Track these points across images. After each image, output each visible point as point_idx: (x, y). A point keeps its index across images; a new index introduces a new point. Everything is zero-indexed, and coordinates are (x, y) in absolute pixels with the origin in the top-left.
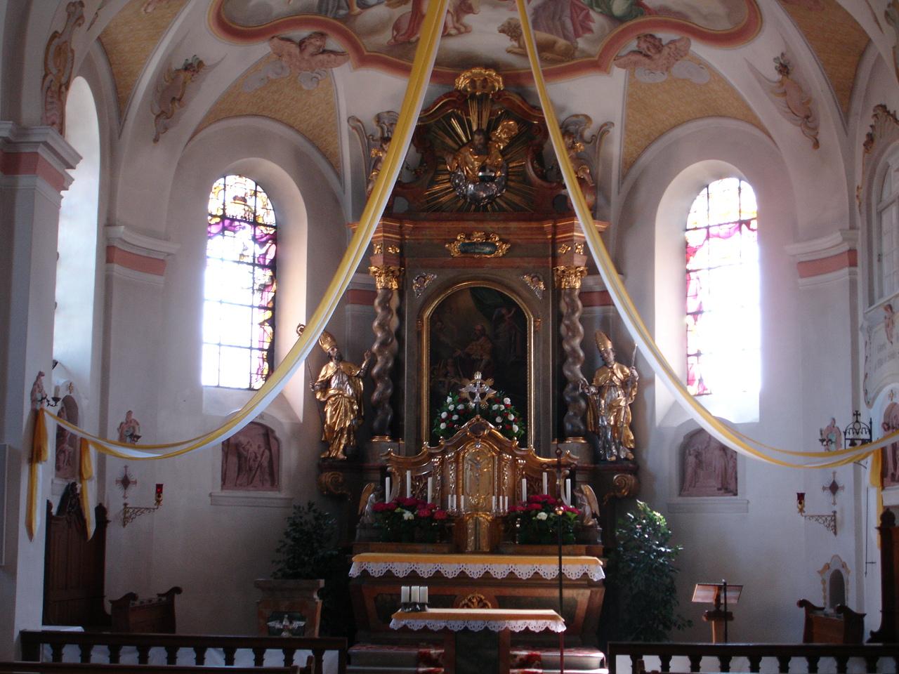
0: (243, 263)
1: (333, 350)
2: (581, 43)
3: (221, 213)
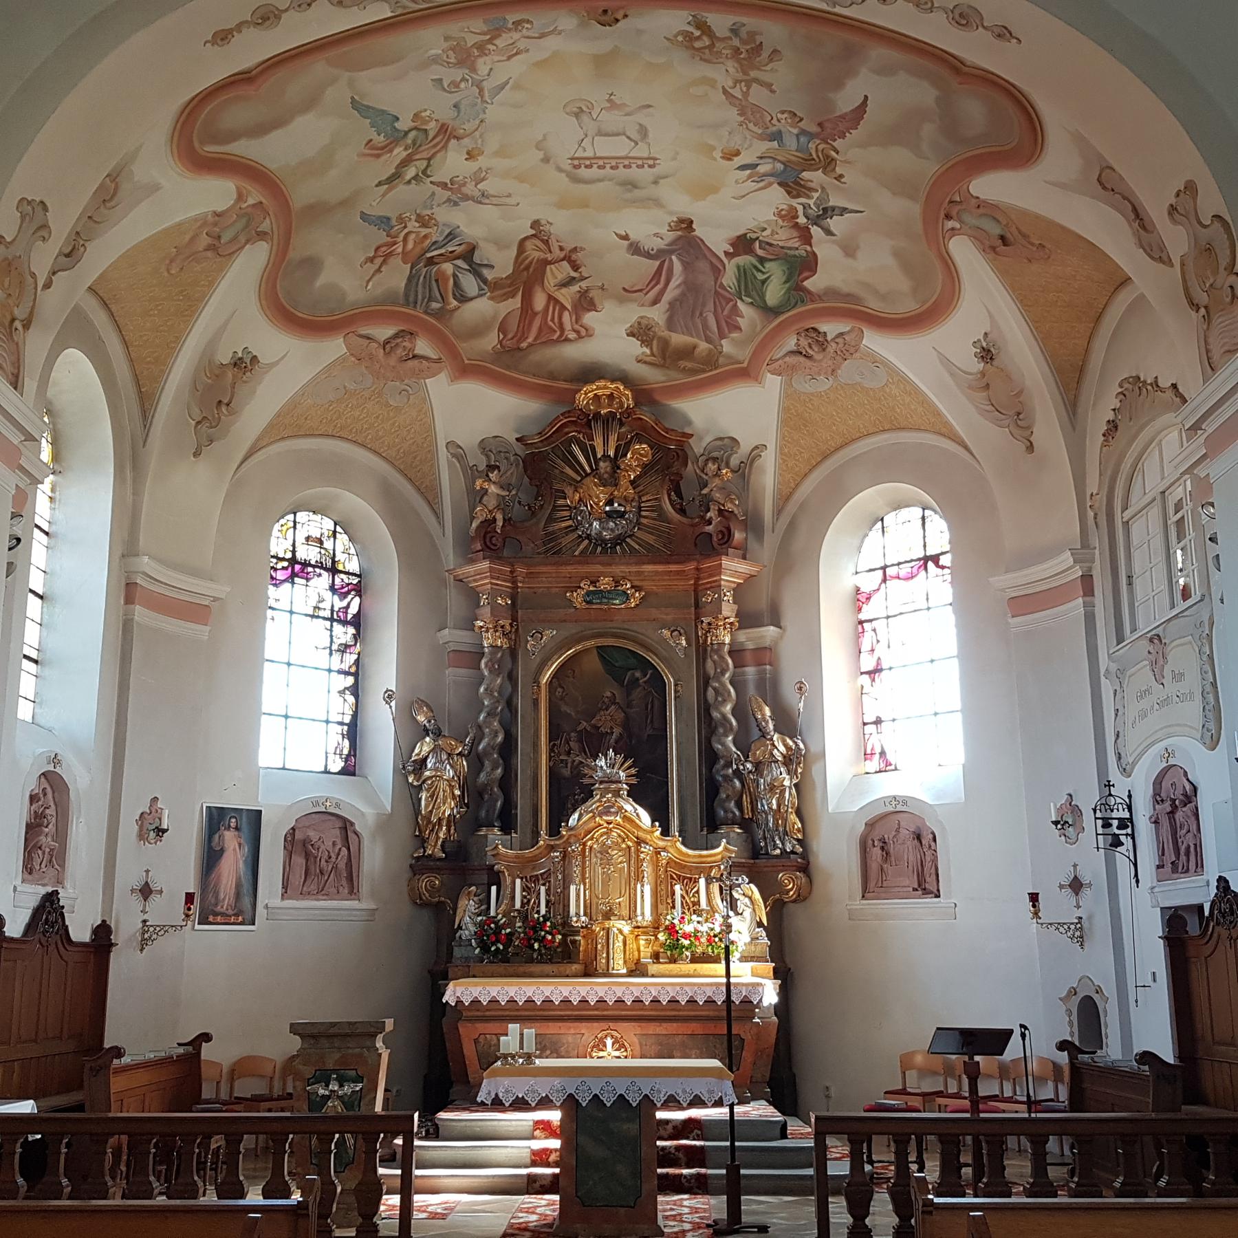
0: (318, 617)
2: (727, 346)
3: (289, 555)
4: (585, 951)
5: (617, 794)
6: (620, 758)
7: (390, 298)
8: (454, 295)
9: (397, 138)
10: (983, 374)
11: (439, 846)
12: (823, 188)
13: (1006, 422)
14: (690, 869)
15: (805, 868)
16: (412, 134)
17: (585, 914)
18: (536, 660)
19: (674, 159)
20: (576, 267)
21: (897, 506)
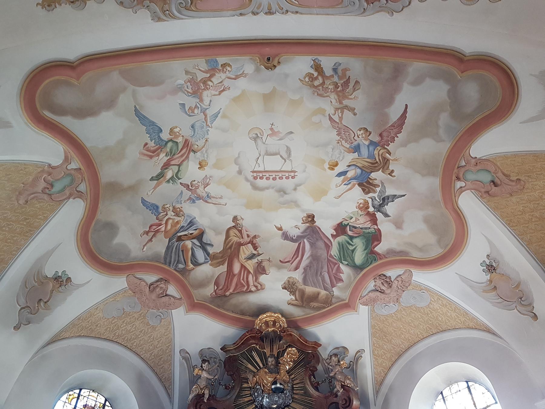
2: (336, 291)
7: (155, 258)
8: (191, 260)
9: (161, 145)
10: (491, 281)
12: (382, 183)
13: (514, 305)
16: (170, 144)
19: (304, 171)
20: (255, 248)
21: (450, 383)
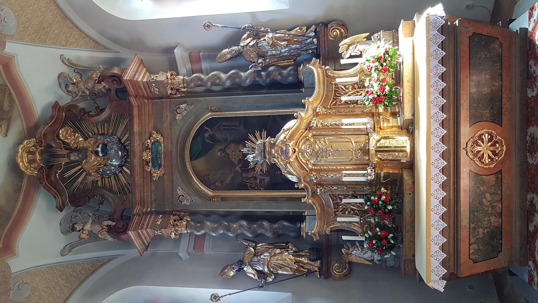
1: (234, 268)
4: (392, 168)
5: (272, 146)
6: (249, 143)
11: (313, 263)
14: (328, 91)
15: (326, 24)
17: (365, 169)
18: (196, 199)
